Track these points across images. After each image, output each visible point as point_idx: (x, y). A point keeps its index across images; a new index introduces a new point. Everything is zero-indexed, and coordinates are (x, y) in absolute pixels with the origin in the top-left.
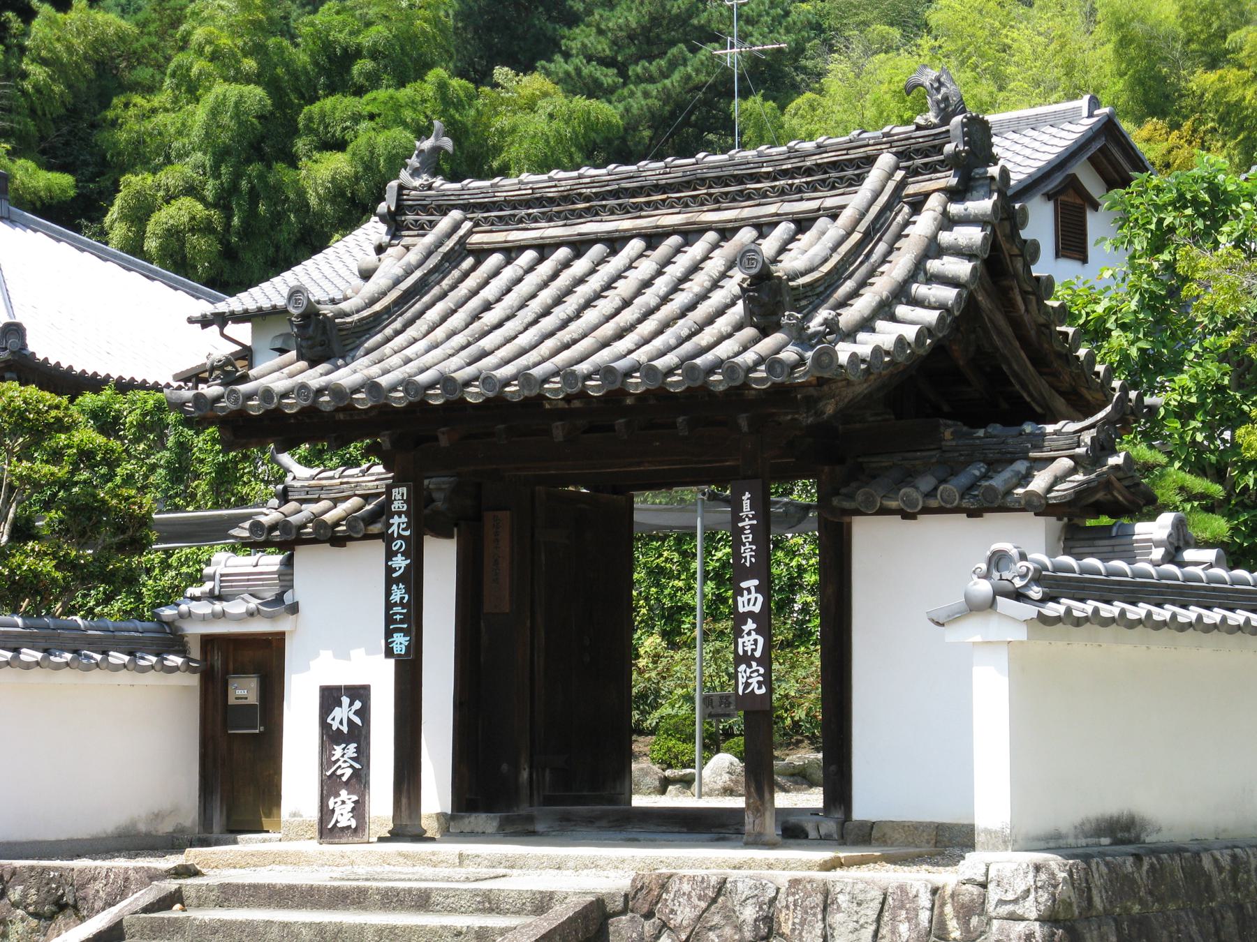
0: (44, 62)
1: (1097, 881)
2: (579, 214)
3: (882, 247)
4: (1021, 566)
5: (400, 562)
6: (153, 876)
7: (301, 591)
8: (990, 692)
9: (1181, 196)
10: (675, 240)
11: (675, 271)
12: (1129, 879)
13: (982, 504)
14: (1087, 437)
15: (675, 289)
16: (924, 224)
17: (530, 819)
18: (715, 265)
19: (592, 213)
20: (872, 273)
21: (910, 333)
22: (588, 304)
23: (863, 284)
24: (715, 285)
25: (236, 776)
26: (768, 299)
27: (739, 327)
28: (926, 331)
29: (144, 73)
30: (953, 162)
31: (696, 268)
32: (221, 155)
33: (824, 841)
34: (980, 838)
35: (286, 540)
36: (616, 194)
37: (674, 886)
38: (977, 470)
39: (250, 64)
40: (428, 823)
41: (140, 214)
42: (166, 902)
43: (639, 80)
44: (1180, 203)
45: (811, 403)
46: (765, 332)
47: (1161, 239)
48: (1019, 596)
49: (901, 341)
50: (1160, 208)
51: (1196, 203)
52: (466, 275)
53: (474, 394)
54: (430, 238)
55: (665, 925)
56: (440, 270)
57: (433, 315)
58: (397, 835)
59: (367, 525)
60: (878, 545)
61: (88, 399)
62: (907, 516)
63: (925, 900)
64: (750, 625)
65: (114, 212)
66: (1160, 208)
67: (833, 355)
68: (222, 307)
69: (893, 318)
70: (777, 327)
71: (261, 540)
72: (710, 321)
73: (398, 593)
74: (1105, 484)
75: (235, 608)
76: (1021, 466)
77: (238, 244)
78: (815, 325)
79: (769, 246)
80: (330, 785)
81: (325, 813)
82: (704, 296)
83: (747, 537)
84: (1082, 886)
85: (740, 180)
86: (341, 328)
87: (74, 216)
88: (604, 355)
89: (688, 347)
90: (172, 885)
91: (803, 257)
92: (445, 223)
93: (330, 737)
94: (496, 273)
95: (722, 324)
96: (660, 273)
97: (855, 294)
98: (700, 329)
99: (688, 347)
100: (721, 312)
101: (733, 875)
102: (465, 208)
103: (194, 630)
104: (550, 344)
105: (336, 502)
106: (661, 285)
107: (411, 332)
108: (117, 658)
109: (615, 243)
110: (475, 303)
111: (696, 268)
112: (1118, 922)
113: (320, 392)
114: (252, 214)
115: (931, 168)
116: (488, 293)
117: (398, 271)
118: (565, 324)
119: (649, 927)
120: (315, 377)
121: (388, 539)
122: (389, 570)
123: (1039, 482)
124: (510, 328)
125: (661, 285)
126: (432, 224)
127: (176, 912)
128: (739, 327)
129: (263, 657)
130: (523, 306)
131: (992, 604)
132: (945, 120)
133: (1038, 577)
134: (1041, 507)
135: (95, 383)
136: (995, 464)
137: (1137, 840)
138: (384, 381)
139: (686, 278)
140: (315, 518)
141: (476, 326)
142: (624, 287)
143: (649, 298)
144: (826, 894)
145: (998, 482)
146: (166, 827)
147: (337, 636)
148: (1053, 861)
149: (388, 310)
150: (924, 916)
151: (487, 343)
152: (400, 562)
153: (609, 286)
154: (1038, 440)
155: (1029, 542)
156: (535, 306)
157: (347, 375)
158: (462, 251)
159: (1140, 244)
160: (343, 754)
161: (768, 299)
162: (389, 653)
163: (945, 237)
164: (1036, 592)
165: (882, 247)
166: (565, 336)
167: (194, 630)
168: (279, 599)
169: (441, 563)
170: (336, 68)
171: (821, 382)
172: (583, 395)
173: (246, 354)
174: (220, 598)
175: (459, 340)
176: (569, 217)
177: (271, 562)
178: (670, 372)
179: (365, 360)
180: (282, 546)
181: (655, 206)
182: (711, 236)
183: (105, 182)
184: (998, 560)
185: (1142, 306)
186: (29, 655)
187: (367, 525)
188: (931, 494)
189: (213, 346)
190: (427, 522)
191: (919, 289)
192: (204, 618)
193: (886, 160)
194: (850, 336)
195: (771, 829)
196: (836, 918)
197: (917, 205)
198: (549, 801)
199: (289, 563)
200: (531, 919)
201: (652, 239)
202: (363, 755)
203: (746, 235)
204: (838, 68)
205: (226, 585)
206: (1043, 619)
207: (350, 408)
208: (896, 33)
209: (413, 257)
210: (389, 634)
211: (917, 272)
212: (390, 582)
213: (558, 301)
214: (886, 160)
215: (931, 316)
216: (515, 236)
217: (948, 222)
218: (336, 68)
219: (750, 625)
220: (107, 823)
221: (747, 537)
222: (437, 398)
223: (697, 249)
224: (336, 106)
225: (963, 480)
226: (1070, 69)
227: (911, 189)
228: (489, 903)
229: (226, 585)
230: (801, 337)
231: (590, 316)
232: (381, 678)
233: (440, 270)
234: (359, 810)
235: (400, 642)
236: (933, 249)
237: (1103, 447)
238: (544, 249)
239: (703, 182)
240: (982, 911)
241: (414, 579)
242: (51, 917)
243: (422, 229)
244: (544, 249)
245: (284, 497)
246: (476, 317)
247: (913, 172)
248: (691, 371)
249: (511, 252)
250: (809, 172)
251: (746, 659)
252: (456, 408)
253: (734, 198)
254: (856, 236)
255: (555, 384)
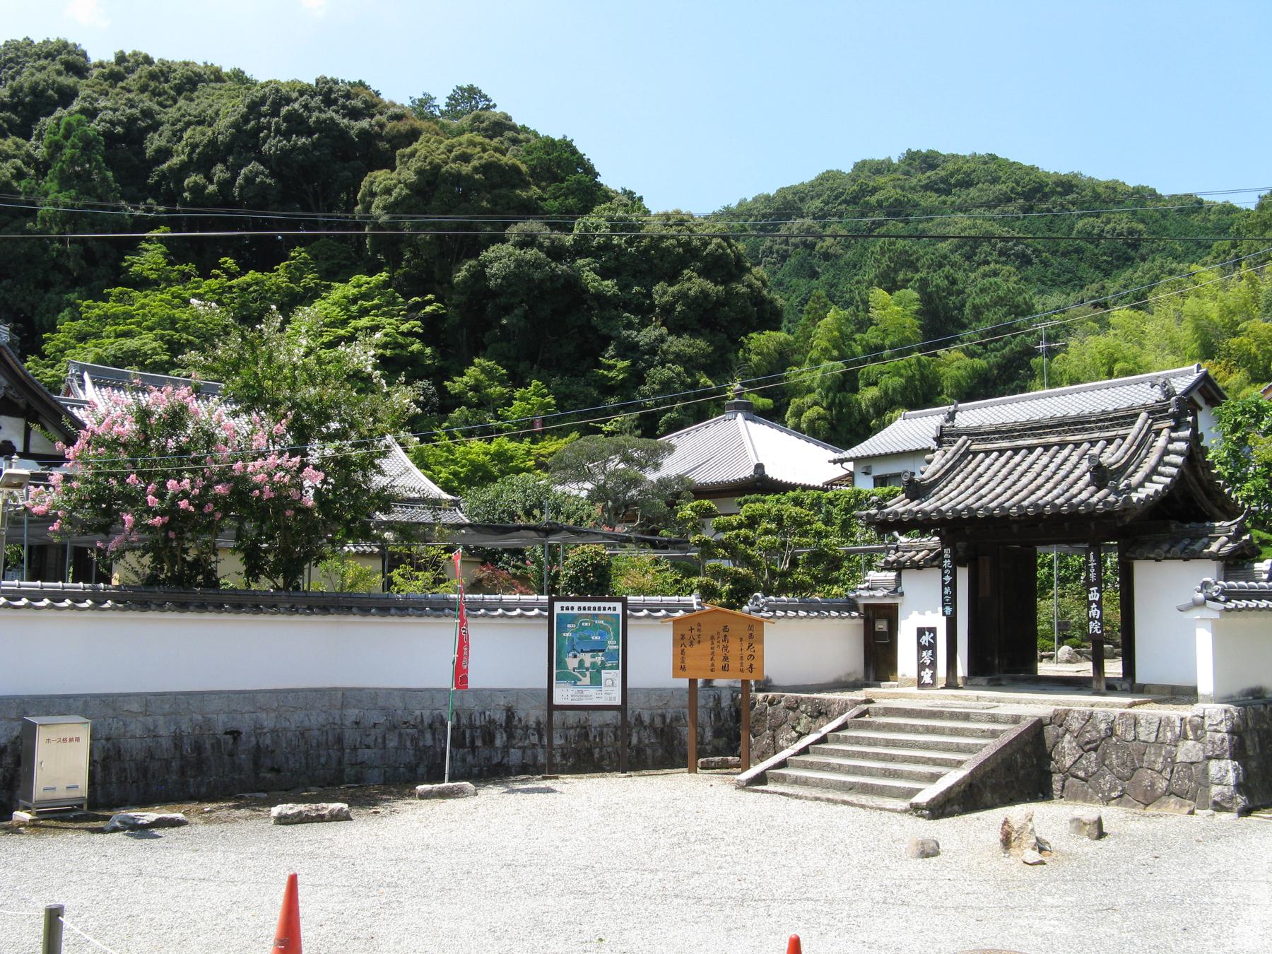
0: (758, 354)
1: (1250, 716)
2: (1015, 437)
3: (1144, 451)
4: (1216, 587)
5: (948, 578)
6: (857, 703)
7: (905, 586)
8: (1204, 640)
9: (1244, 409)
10: (1056, 448)
11: (1058, 460)
12: (1262, 715)
13: (1190, 555)
14: (1233, 528)
15: (1058, 469)
16: (1161, 442)
17: (999, 679)
18: (1074, 459)
19: (1021, 437)
20: (1141, 462)
21: (1160, 487)
22: (1022, 475)
23: (1138, 467)
24: (1075, 467)
25: (879, 659)
26: (1101, 476)
27: (1088, 486)
28: (1166, 486)
29: (797, 357)
30: (1172, 416)
31: (1066, 460)
32: (829, 389)
33: (1124, 692)
34: (1200, 698)
35: (899, 567)
36: (1030, 429)
37: (1071, 714)
38: (1186, 542)
39: (835, 353)
40: (959, 681)
41: (799, 413)
42: (862, 714)
43: (993, 350)
44: (1244, 412)
45: (1121, 518)
46: (1099, 489)
47: (1236, 427)
48: (1215, 599)
49: (1156, 491)
50: (1235, 414)
51: (1250, 411)
52: (970, 462)
53: (981, 513)
54: (954, 448)
55: (1067, 730)
56: (959, 461)
57: (958, 479)
58: (948, 686)
59: (934, 561)
60: (1144, 572)
61: (791, 494)
62: (1157, 560)
63: (1178, 723)
64: (1094, 605)
65: (788, 413)
66: (1235, 414)
67: (1130, 498)
68: (842, 456)
69: (1152, 481)
70: (1105, 486)
71: (888, 567)
72: (1075, 482)
73: (947, 591)
74: (1241, 547)
75: (879, 593)
76: (1205, 540)
77: (842, 428)
78: (1122, 486)
79: (1096, 450)
80: (921, 667)
81: (920, 677)
82: (1071, 472)
83: (1092, 570)
84: (1243, 718)
85: (1082, 423)
86: (923, 486)
87: (774, 416)
88: (1033, 498)
89: (1067, 495)
90: (865, 707)
91: (1111, 457)
92: (960, 441)
93: (921, 648)
94: (983, 461)
95: (1081, 484)
96: (1051, 461)
97: (1135, 471)
98: (1071, 487)
99: (1067, 495)
100: (1079, 479)
101: (1095, 709)
102: (968, 435)
103: (861, 602)
104: (1009, 492)
105: (918, 552)
106: (1052, 467)
107: (951, 486)
108: (834, 614)
109: (1031, 449)
110: (975, 474)
111: (1066, 460)
112: (1258, 731)
113: (917, 512)
114: (840, 412)
115: (1163, 418)
116: (980, 470)
117: (943, 461)
118: (1014, 484)
119: (1061, 730)
120: (914, 506)
121: (943, 569)
122: (943, 581)
123: (1214, 547)
124: (992, 484)
125: (1052, 467)
126: (955, 442)
127: (867, 718)
128: (1088, 486)
129: (890, 613)
130: (995, 475)
131: (1204, 603)
132: (1168, 399)
133: (1223, 592)
134: (1214, 557)
135: (793, 487)
136: (1195, 539)
137: (1263, 697)
138: (943, 508)
139: (1062, 464)
140: (910, 558)
141: (977, 484)
142: (1037, 468)
143: (1048, 472)
144: (1136, 720)
145: (1196, 547)
146: (852, 679)
147: (923, 611)
148: (1232, 708)
149: (940, 478)
150: (1178, 730)
151: (983, 492)
152: (948, 578)
153: (1030, 467)
154: (1213, 529)
155: (1208, 572)
156: (1001, 475)
157: (928, 505)
158: (968, 452)
159: (1228, 428)
160: (926, 655)
161: (1101, 476)
162: (944, 614)
163: (1171, 447)
164: (1222, 598)
165: (1144, 451)
166: (1015, 489)
167: (861, 602)
168: (895, 590)
169: (963, 575)
170: (875, 353)
171: (1125, 510)
172: (1026, 514)
173: (851, 474)
174: (872, 589)
175: (971, 490)
176: (1011, 438)
177: (892, 575)
178: (1062, 505)
179: (933, 499)
180: (896, 570)
181: (1047, 434)
182: (1071, 446)
183: (785, 400)
184: (1205, 585)
185: (1229, 455)
186: (802, 613)
187: (934, 561)
188: (1168, 551)
189: (838, 471)
190: (957, 562)
191: (1161, 469)
192: (866, 598)
193: (1144, 415)
194: (1135, 490)
195: (1103, 687)
196: (1140, 729)
197: (1158, 433)
198: (1006, 672)
199: (899, 576)
200: (1012, 726)
201: (1047, 448)
202: (934, 655)
203: (1086, 446)
204: (1073, 342)
205: (875, 583)
206: (1226, 610)
207: (930, 519)
208: (1096, 326)
209: (948, 456)
210: (944, 607)
211: (1160, 462)
212: (944, 586)
213: (1010, 473)
214: (1144, 415)
215: (1168, 480)
216: (989, 446)
217: (1171, 440)
218: (875, 353)
219: (1094, 605)
220: (829, 677)
221: (1092, 570)
222: (965, 515)
223: (1066, 452)
224: (872, 368)
225: (1181, 546)
226: (1172, 340)
227: (1155, 427)
228: (994, 719)
229: (875, 583)
230: (1117, 492)
231: (1024, 480)
232: (941, 625)
233: (959, 461)
234: (933, 676)
235: (948, 610)
236: (1166, 452)
237: (1241, 531)
238: (1002, 452)
239: (1067, 424)
240: (1202, 728)
241: (953, 585)
242: (817, 717)
243: (951, 443)
244: (1002, 452)
245: (897, 550)
246: (976, 480)
247: (1155, 420)
248: (1071, 505)
249: (988, 453)
250: (1111, 420)
251: (1093, 619)
252: (973, 519)
253: (1080, 431)
254: (1134, 448)
255: (1014, 510)
